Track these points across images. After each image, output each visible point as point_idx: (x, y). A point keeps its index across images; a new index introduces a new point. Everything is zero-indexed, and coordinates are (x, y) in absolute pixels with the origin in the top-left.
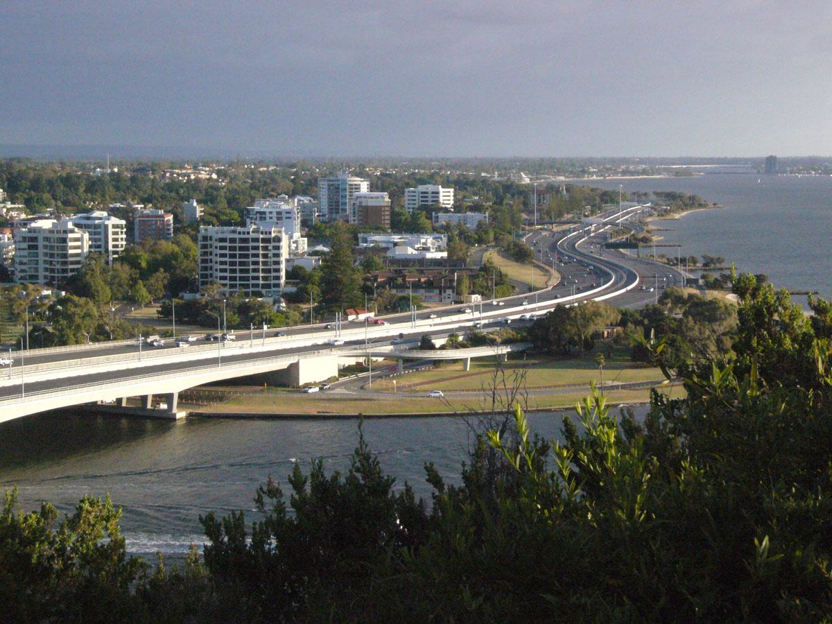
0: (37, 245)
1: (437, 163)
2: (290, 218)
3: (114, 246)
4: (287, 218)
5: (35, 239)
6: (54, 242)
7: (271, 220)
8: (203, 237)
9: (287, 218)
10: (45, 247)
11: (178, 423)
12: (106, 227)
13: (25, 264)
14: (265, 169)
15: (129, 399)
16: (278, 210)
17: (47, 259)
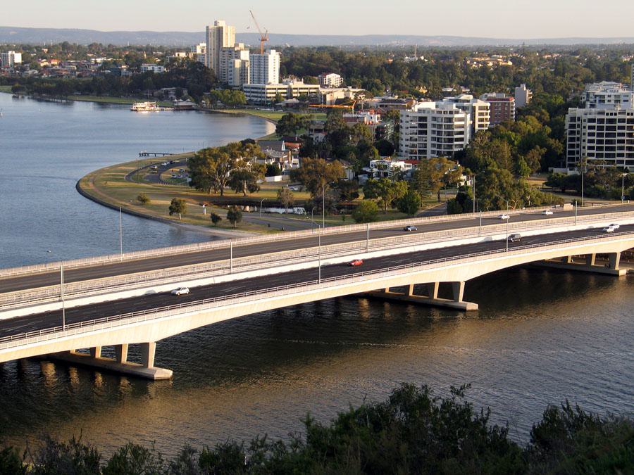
0: (426, 124)
1: (14, 32)
2: (627, 101)
3: (480, 126)
4: (624, 101)
5: (424, 119)
6: (442, 121)
7: (609, 103)
8: (571, 118)
9: (624, 101)
10: (434, 125)
11: (621, 279)
12: (474, 108)
13: (416, 140)
14: (550, 56)
15: (573, 257)
16: (616, 94)
17: (435, 136)
